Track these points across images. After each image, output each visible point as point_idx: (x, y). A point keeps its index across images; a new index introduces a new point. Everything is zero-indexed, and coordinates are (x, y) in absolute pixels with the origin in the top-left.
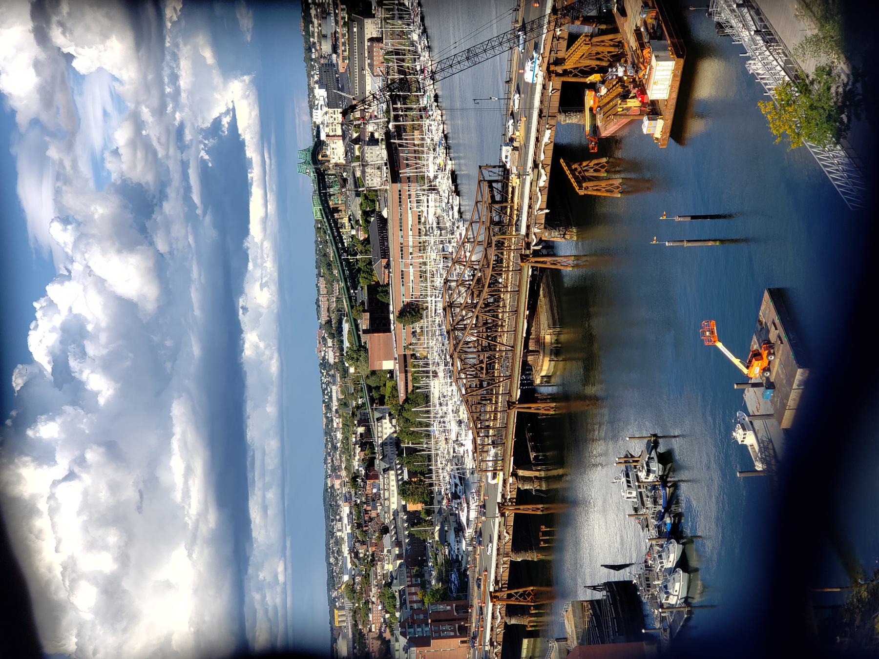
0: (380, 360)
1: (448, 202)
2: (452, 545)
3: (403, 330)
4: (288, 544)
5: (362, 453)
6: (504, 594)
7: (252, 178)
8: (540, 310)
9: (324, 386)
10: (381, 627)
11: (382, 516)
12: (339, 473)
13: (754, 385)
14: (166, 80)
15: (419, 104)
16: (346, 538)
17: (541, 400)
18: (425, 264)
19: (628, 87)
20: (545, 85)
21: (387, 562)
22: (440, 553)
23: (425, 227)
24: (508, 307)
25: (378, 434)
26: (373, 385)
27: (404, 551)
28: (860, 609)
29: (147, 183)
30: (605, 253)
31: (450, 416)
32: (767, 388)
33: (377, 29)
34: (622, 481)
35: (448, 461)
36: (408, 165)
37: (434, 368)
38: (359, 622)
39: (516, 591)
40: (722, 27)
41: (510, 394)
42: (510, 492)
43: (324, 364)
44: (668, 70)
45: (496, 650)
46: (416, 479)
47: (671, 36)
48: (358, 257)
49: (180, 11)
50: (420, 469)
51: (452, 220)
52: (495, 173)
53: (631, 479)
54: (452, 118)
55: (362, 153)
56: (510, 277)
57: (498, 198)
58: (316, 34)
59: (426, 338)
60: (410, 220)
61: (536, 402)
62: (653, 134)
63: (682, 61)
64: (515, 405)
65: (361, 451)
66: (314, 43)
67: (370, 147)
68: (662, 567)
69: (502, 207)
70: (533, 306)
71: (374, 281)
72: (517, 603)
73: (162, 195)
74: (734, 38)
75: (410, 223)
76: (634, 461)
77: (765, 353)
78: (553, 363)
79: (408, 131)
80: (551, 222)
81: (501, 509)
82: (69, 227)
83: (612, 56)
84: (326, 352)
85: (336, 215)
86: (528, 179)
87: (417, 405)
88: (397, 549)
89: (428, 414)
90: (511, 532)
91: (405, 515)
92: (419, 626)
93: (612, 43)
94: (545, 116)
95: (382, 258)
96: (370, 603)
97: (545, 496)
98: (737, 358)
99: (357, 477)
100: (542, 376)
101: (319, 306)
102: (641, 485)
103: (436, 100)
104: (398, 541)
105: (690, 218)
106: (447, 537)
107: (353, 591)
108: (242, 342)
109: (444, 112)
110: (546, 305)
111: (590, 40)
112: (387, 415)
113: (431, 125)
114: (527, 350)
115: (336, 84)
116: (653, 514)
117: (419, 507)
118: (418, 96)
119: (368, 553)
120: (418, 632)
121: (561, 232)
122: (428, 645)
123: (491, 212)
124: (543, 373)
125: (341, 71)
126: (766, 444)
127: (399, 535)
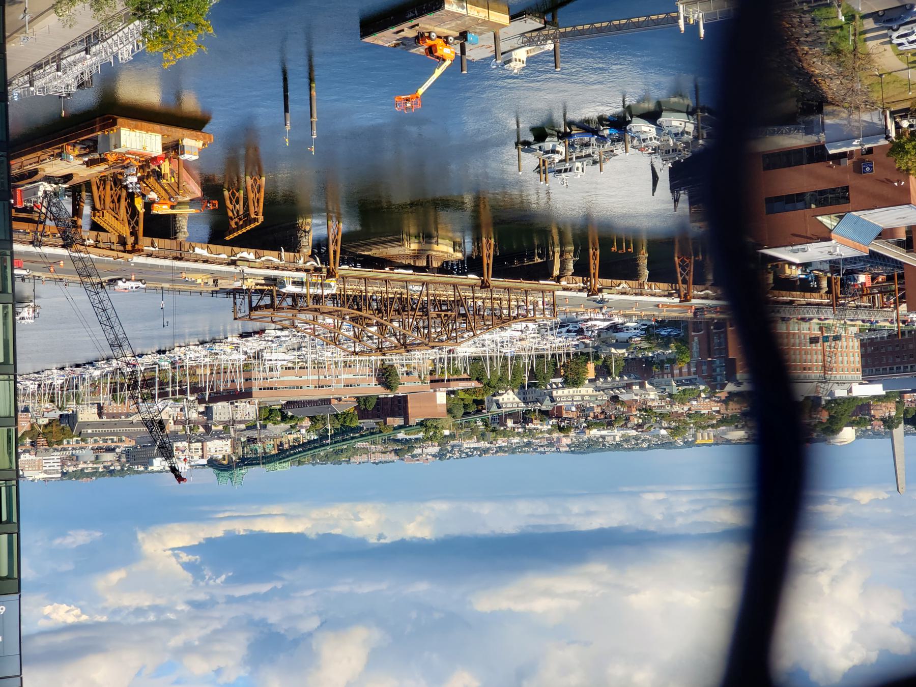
0: (436, 406)
1: (272, 341)
2: (630, 335)
3: (405, 385)
4: (626, 489)
5: (535, 421)
6: (683, 288)
7: (244, 530)
8: (384, 254)
9: (463, 455)
10: (714, 401)
11: (600, 403)
12: (555, 440)
14: (142, 620)
15: (168, 369)
16: (622, 432)
17: (479, 252)
19: (148, 172)
20: (147, 254)
21: (647, 396)
22: (639, 345)
23: (298, 362)
24: (382, 289)
25: (515, 407)
26: (463, 411)
27: (637, 381)
30: (324, 189)
32: (466, 40)
33: (89, 408)
34: (564, 177)
36: (233, 381)
37: (444, 353)
39: (679, 275)
40: (83, 84)
41: (473, 286)
42: (576, 283)
43: (441, 456)
44: (130, 135)
46: (562, 371)
47: (93, 131)
48: (329, 428)
49: (70, 606)
50: (551, 366)
51: (290, 337)
52: (241, 303)
53: (563, 168)
54: (182, 336)
55: (220, 422)
56: (351, 287)
57: (267, 300)
58: (95, 466)
59: (414, 361)
60: (290, 378)
62: (199, 149)
63: (120, 120)
64: (485, 281)
65: (532, 423)
66: (105, 467)
67: (214, 416)
68: (655, 138)
69: (277, 295)
71: (354, 411)
72: (692, 273)
74: (94, 72)
75: (294, 378)
76: (544, 165)
77: (429, 42)
78: (440, 241)
79: (196, 381)
80: (293, 246)
81: (594, 292)
83: (115, 184)
84: (427, 454)
85: (286, 446)
86: (248, 270)
87: (483, 369)
88: (634, 387)
89: (493, 359)
90: (619, 281)
91: (599, 380)
92: (715, 370)
93: (101, 188)
94: (181, 254)
95: (330, 403)
96: (690, 412)
97: (580, 247)
98: (433, 73)
99: (559, 426)
100: (454, 251)
101: (380, 462)
102: (568, 157)
103: (164, 352)
104: (626, 387)
105: (287, 114)
106: (623, 341)
107: (677, 428)
108: (414, 540)
109: (177, 345)
110: (379, 249)
111: (99, 211)
112: (494, 398)
113: (190, 358)
115: (148, 448)
116: (599, 146)
117: (591, 366)
118: (159, 370)
119: (638, 415)
120: (721, 371)
121: (303, 235)
123: (283, 309)
124: (451, 250)
125: (134, 444)
126: (525, 40)
127: (620, 385)
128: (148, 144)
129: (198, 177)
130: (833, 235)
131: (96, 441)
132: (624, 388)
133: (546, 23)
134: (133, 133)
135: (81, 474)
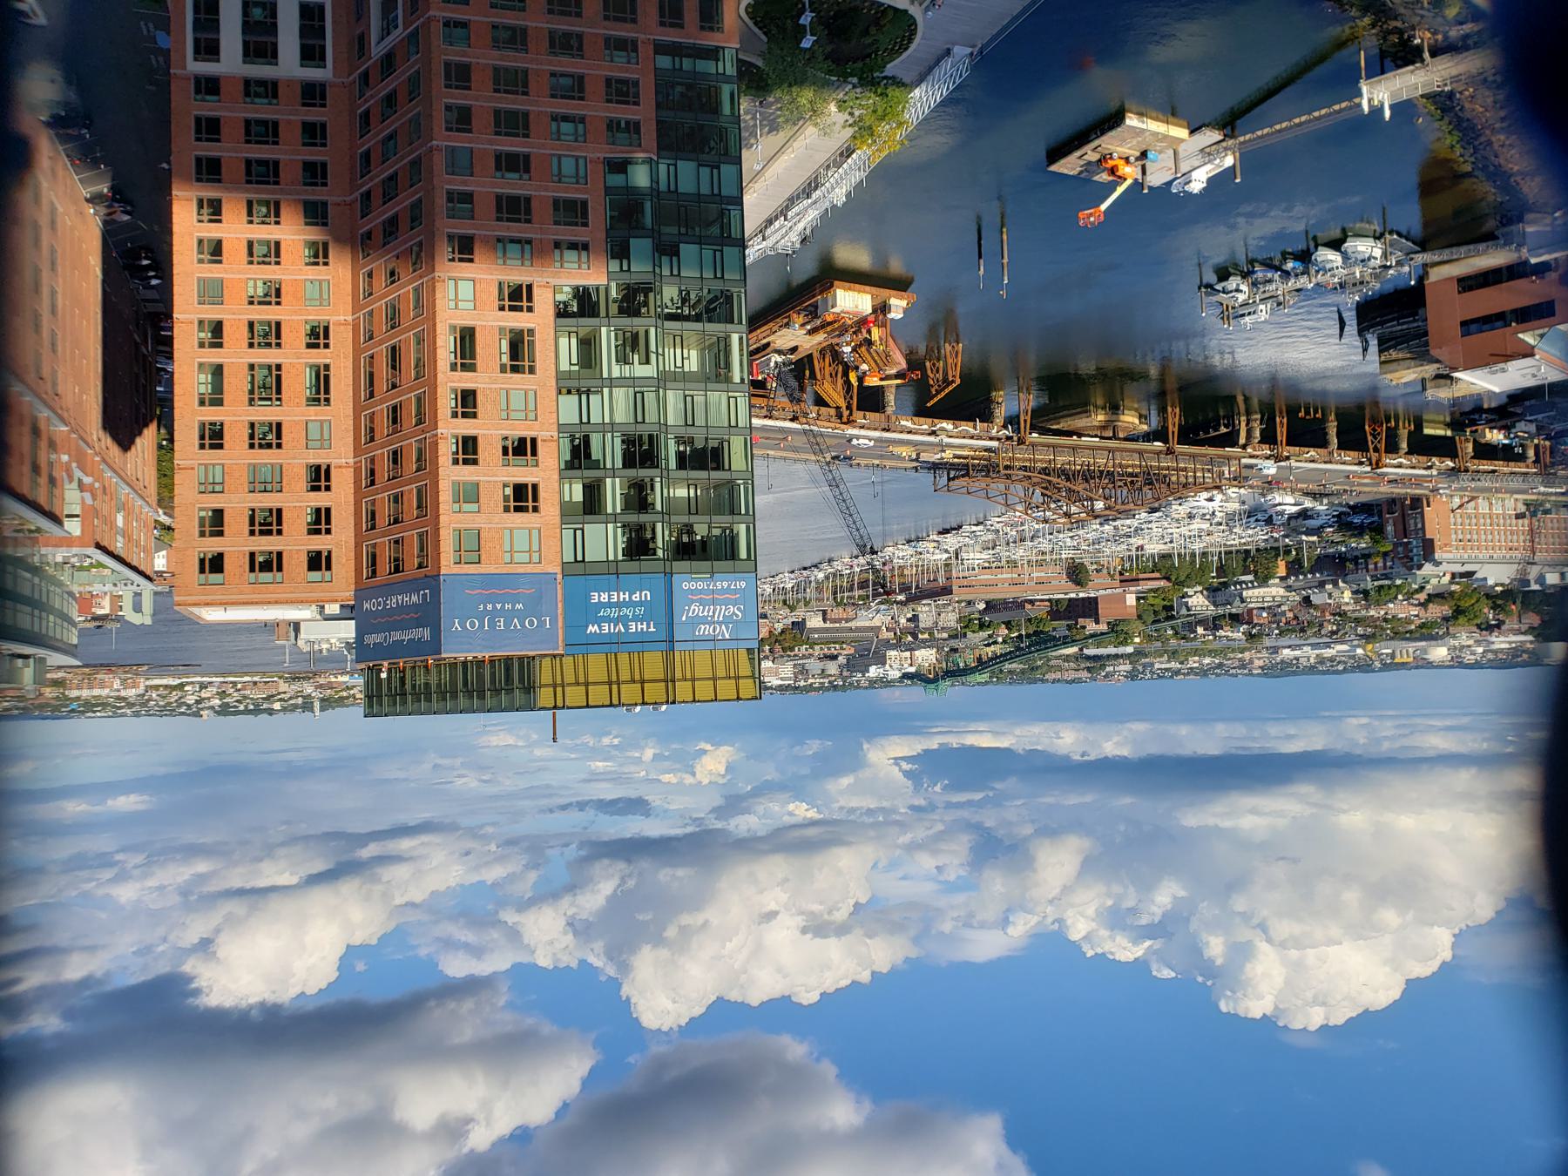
0: (1126, 607)
4: (1327, 714)
5: (1226, 629)
6: (1374, 456)
9: (1155, 676)
13: (1144, 172)
17: (1164, 422)
18: (1029, 561)
28: (1383, 23)
29: (970, 841)
31: (1184, 531)
35: (1231, 531)
38: (1408, 629)
39: (1370, 443)
41: (1158, 453)
43: (1132, 676)
45: (1437, 463)
47: (814, 296)
60: (986, 577)
61: (1167, 428)
63: (836, 283)
66: (829, 682)
70: (1069, 434)
73: (977, 828)
75: (990, 577)
78: (1126, 412)
80: (987, 417)
82: (1011, 919)
83: (834, 362)
88: (1327, 586)
90: (1307, 449)
92: (1411, 551)
98: (1115, 190)
99: (1250, 633)
114: (1115, 437)
122: (1432, 541)
128: (860, 303)
129: (903, 348)
130: (1536, 350)
131: (821, 649)
132: (1316, 587)
133: (1225, 135)
134: (847, 294)
135: (810, 689)
